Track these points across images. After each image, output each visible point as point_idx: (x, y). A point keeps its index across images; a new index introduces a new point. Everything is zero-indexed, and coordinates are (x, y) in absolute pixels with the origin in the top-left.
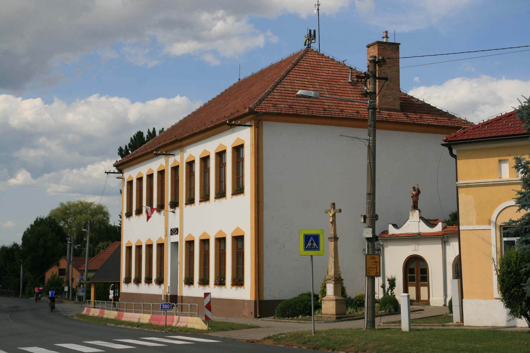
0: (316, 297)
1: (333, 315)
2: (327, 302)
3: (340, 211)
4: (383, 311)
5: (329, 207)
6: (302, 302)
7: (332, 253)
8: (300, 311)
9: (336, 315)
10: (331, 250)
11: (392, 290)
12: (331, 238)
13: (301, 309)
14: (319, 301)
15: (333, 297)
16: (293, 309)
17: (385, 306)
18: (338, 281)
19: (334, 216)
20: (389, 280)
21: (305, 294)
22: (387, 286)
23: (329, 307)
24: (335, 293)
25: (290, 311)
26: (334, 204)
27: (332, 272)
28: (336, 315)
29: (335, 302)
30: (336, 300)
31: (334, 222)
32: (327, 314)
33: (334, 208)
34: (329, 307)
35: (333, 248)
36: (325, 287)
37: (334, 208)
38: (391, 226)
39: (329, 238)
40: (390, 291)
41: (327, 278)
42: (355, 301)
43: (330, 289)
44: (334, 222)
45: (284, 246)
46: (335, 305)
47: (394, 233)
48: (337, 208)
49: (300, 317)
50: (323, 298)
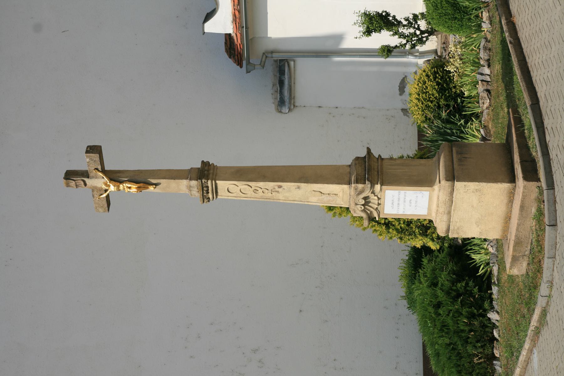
0: (418, 256)
1: (511, 195)
2: (455, 217)
3: (94, 149)
4: (485, 15)
5: (77, 193)
6: (438, 306)
7: (264, 189)
8: (472, 316)
9: (512, 179)
10: (249, 192)
11: (399, 23)
12: (204, 189)
13: (464, 311)
14: (433, 246)
15: (440, 189)
16: (466, 341)
17: (465, 11)
18: (370, 170)
19: (115, 177)
20: (368, 32)
21: (410, 292)
22: (385, 38)
23: (474, 210)
24: (424, 181)
25: (470, 349)
26: (70, 175)
27: (340, 194)
28: (512, 179)
29: (458, 184)
30: (452, 177)
31: (142, 179)
32: (508, 219)
33: (85, 174)
34: (474, 210)
35: (242, 185)
36: (388, 224)
37: (85, 174)
38: (211, 27)
39: (205, 198)
40: (401, 30)
41: (358, 212)
42: (437, 123)
43: (402, 202)
44: (142, 179)
45: (255, 351)
46: (472, 186)
47: (230, 18)
48: (83, 162)
49: (493, 316)
50: (441, 231)
